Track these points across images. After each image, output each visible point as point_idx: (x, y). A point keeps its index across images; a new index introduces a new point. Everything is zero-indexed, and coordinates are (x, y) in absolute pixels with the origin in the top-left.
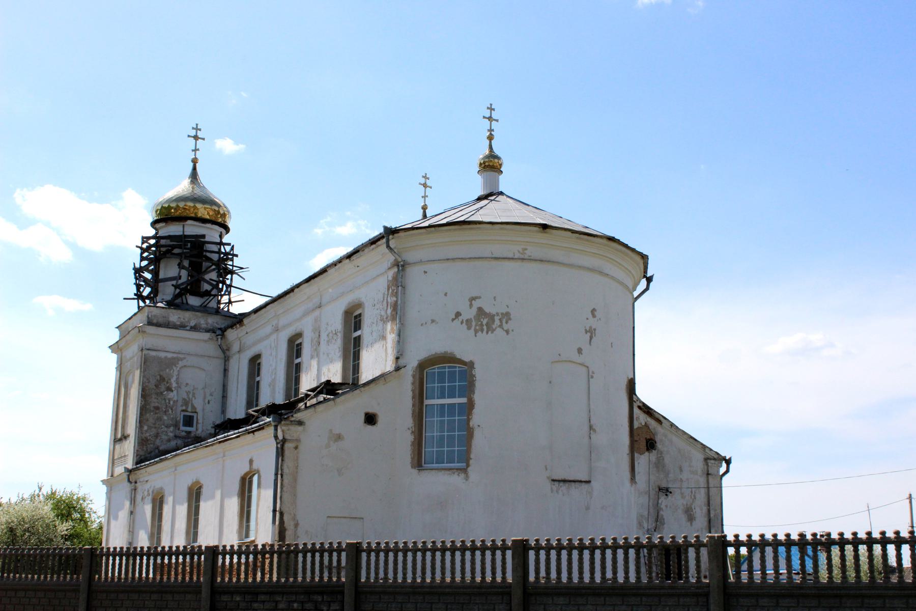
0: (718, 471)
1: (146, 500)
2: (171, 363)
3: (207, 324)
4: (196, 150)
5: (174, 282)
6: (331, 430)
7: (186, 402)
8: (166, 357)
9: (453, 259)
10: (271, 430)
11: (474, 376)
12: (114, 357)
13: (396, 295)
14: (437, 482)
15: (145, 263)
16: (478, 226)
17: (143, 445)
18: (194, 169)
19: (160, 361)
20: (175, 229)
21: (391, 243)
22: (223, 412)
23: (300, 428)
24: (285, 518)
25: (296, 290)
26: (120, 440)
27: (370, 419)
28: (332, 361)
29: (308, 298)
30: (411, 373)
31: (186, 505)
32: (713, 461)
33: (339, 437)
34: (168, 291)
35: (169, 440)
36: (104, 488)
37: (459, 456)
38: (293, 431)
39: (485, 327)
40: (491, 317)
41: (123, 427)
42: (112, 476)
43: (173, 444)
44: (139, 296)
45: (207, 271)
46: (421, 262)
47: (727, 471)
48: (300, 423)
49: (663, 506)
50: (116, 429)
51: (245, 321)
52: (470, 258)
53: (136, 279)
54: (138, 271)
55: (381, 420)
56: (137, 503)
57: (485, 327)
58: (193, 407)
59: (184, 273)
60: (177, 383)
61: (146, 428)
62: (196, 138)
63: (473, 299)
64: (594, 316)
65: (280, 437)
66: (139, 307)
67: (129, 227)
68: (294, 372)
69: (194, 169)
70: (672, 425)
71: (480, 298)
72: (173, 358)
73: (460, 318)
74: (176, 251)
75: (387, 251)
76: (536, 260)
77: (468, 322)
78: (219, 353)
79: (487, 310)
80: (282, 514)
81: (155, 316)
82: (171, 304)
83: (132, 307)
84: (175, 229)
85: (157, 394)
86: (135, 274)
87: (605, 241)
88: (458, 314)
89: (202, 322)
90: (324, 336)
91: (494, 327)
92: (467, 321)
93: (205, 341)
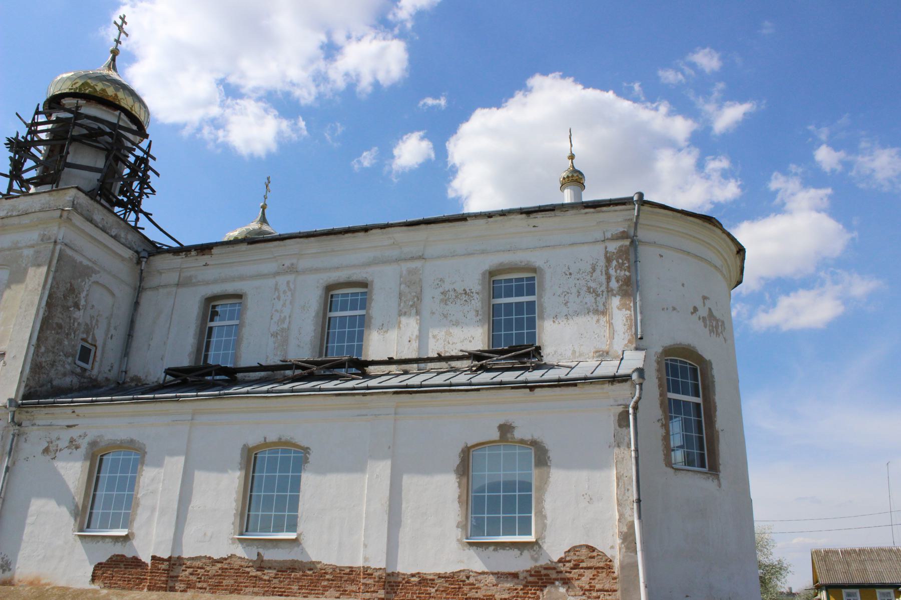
8: (81, 262)
30: (655, 358)
35: (65, 375)
43: (68, 381)
58: (94, 338)
60: (86, 301)
61: (43, 349)
72: (87, 267)
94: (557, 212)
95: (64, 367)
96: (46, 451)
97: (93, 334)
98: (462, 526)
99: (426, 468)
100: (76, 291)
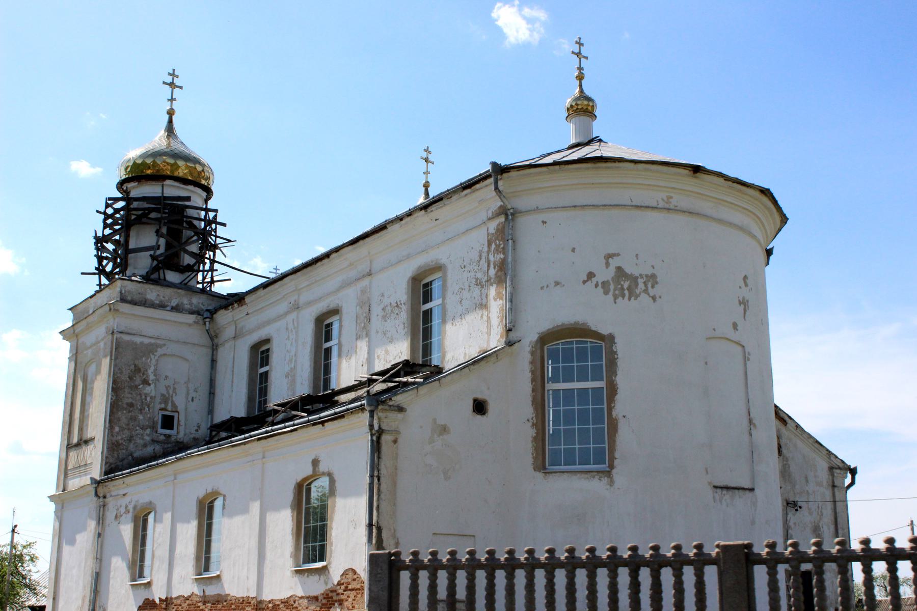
0: (843, 483)
1: (123, 519)
2: (150, 350)
3: (191, 304)
4: (172, 100)
5: (152, 252)
6: (435, 420)
7: (165, 399)
8: (142, 343)
9: (583, 207)
10: (366, 416)
11: (615, 353)
12: (67, 345)
13: (504, 251)
14: (571, 489)
15: (108, 231)
16: (617, 164)
17: (114, 450)
18: (170, 121)
19: (135, 347)
20: (151, 190)
21: (500, 183)
22: (211, 411)
23: (400, 416)
24: (384, 535)
25: (333, 256)
26: (78, 445)
27: (480, 407)
28: (391, 340)
29: (351, 265)
30: (528, 349)
31: (194, 524)
32: (838, 471)
33: (444, 430)
34: (142, 263)
35: (145, 446)
36: (52, 506)
37: (600, 458)
38: (389, 420)
39: (626, 292)
40: (634, 279)
41: (81, 429)
42: (64, 490)
43: (150, 450)
44: (101, 271)
45: (188, 242)
46: (537, 210)
47: (853, 483)
48: (401, 409)
49: (791, 524)
50: (70, 432)
51: (248, 299)
52: (605, 205)
53: (97, 249)
54: (100, 241)
55: (492, 407)
56: (107, 522)
57: (626, 292)
58: (174, 405)
59: (162, 242)
60: (155, 375)
61: (117, 429)
62: (172, 85)
63: (609, 256)
64: (746, 285)
65: (376, 427)
66: (100, 285)
67: (96, 182)
68: (323, 361)
69: (170, 121)
70: (798, 426)
71: (618, 255)
72: (151, 344)
73: (594, 280)
74: (153, 215)
75: (494, 193)
76: (684, 212)
77: (605, 285)
78: (205, 340)
79: (628, 270)
80: (379, 529)
81: (129, 292)
82: (147, 279)
83: (92, 284)
84: (151, 190)
85: (131, 387)
86: (96, 244)
87: (757, 194)
88: (591, 275)
89: (186, 301)
90: (377, 311)
91: (638, 292)
92: (603, 283)
93: (190, 325)
94: (445, 201)
95: (143, 439)
96: (116, 517)
97: (173, 402)
98: (295, 555)
99: (277, 508)
100: (142, 370)
